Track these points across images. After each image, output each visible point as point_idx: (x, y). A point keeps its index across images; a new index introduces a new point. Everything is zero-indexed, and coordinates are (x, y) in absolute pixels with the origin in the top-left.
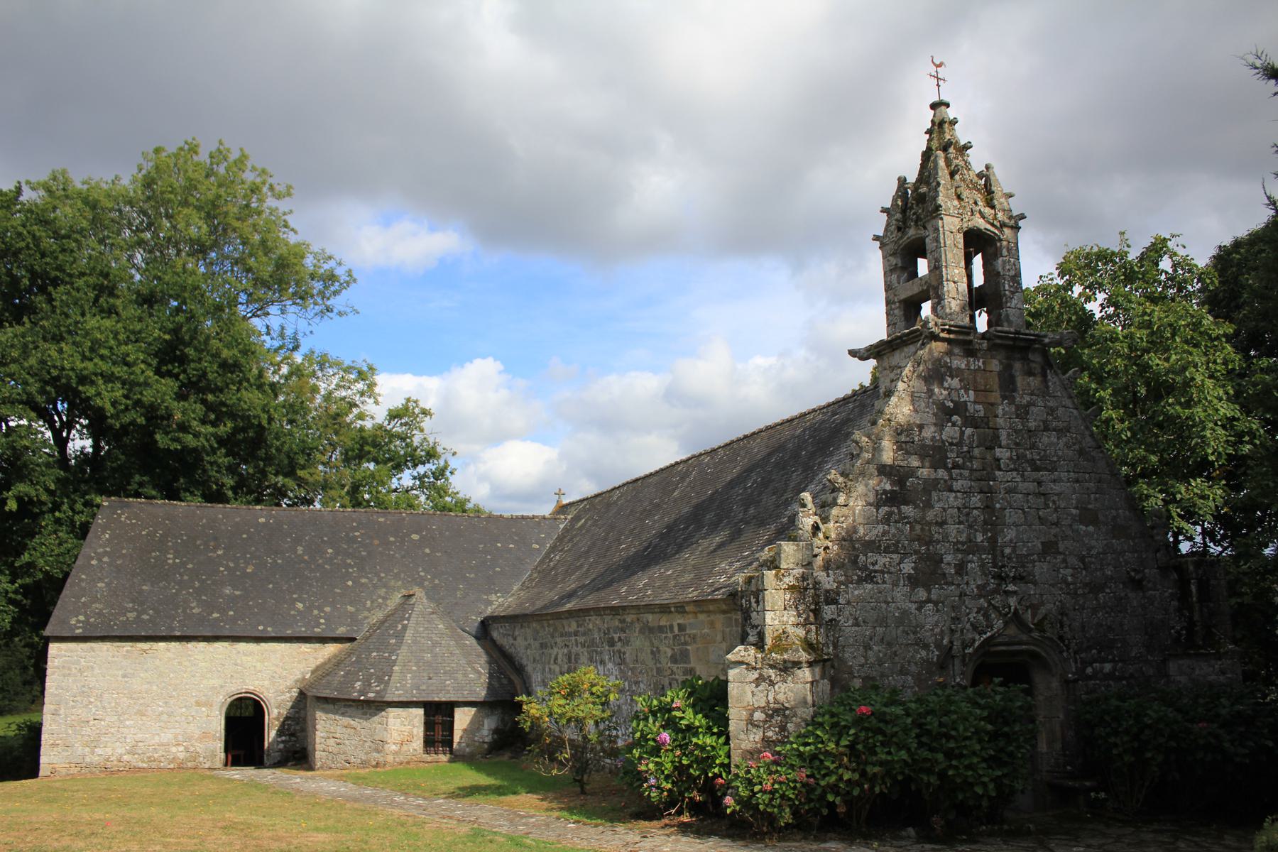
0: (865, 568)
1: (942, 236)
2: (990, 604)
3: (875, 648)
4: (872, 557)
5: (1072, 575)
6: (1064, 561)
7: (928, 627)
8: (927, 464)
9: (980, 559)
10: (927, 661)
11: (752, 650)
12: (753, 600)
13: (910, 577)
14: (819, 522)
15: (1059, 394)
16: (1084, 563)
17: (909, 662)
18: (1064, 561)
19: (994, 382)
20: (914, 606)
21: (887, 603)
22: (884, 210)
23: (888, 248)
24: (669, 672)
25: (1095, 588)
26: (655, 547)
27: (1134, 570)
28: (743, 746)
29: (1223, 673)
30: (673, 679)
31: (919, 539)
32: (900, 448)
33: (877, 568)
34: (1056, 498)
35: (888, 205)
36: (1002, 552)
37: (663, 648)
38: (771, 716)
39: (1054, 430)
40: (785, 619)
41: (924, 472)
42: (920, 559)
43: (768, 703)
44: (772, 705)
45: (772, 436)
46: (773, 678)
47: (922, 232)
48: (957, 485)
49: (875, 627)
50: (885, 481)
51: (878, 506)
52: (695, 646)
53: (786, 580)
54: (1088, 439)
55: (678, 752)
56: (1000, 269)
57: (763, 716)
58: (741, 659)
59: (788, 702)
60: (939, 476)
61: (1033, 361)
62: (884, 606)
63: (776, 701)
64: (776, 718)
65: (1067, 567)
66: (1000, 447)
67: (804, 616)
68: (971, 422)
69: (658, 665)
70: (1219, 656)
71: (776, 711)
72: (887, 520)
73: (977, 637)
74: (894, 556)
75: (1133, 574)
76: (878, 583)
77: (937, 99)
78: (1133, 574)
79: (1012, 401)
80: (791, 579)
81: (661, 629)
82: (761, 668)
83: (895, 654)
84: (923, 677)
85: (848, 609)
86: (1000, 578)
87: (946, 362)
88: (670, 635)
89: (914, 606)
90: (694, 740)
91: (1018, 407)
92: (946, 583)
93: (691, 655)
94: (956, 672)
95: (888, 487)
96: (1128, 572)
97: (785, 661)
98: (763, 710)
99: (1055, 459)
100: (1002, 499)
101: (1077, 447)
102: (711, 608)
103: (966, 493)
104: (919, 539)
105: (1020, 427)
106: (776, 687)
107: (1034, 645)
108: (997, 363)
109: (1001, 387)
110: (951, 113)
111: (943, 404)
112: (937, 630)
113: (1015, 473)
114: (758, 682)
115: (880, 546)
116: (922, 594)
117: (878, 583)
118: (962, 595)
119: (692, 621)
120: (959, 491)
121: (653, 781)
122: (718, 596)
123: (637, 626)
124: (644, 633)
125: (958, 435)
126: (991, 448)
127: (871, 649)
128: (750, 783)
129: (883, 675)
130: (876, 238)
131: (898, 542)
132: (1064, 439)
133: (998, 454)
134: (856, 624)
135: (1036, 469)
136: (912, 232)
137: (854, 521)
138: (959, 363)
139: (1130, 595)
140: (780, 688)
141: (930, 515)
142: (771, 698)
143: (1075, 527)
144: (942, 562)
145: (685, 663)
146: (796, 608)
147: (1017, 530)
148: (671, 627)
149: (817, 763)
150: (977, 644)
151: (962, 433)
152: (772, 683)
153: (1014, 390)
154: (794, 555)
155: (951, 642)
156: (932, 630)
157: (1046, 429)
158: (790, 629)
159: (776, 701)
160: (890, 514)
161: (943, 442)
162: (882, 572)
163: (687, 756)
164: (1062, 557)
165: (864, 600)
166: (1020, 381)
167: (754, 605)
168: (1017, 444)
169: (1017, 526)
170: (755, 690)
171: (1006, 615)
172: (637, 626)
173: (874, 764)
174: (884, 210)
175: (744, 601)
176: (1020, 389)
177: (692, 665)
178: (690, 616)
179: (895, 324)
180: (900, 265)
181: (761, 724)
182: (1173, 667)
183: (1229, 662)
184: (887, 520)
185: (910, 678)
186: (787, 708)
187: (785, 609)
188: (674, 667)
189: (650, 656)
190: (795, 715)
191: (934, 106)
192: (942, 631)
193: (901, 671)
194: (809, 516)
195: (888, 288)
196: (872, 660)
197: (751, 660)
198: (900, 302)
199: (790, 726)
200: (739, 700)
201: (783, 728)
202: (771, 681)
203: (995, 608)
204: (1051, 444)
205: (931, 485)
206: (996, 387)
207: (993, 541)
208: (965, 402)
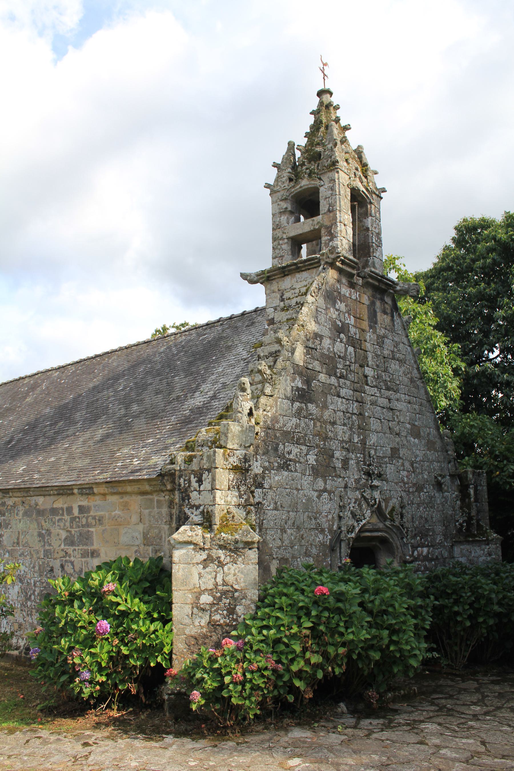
0: (282, 456)
1: (337, 186)
2: (363, 496)
3: (289, 531)
4: (289, 447)
5: (407, 477)
6: (403, 465)
7: (324, 514)
8: (324, 370)
9: (356, 456)
10: (323, 544)
11: (199, 530)
12: (193, 480)
13: (313, 467)
14: (253, 408)
15: (400, 332)
16: (413, 467)
17: (311, 545)
18: (403, 465)
19: (365, 314)
20: (316, 494)
21: (298, 490)
22: (275, 165)
23: (279, 195)
24: (62, 554)
25: (419, 488)
26: (20, 440)
27: (440, 475)
28: (187, 632)
29: (490, 555)
30: (66, 561)
31: (318, 434)
32: (308, 353)
33: (291, 457)
34: (398, 413)
35: (279, 162)
36: (369, 453)
37: (55, 530)
38: (220, 599)
39: (398, 360)
40: (229, 499)
41: (322, 377)
42: (319, 452)
43: (216, 585)
44: (220, 588)
45: (131, 354)
46: (222, 559)
47: (317, 183)
48: (343, 392)
49: (289, 512)
50: (298, 379)
51: (293, 401)
52: (100, 528)
53: (231, 460)
54: (415, 371)
55: (116, 641)
56: (370, 226)
57: (481, 600)
58: (190, 539)
59: (238, 583)
60: (332, 383)
61: (387, 303)
62: (295, 492)
63: (225, 583)
64: (224, 600)
65: (404, 470)
66: (368, 366)
67: (245, 497)
68: (352, 342)
69: (47, 547)
70: (488, 542)
71: (224, 593)
72: (298, 414)
73: (356, 524)
74: (303, 448)
75: (440, 478)
76: (292, 471)
77: (321, 87)
78: (440, 478)
79: (375, 332)
80: (235, 459)
81: (54, 511)
82: (210, 549)
83: (302, 537)
84: (320, 559)
85: (271, 493)
86: (369, 474)
87: (337, 287)
88: (66, 517)
89: (316, 494)
90: (134, 627)
91: (378, 336)
92: (336, 476)
93: (95, 538)
94: (342, 554)
95: (300, 385)
96: (436, 477)
97: (236, 542)
98: (210, 592)
99: (398, 382)
100: (369, 409)
101: (409, 376)
102: (129, 489)
103: (347, 399)
104: (318, 434)
105: (379, 353)
106: (226, 568)
107: (386, 532)
108: (367, 298)
109: (369, 318)
110: (335, 100)
111: (335, 322)
112: (330, 517)
113: (376, 389)
114: (205, 563)
115: (293, 437)
116: (320, 484)
117: (292, 471)
118: (346, 487)
119: (98, 502)
120: (343, 398)
121: (87, 675)
122: (144, 475)
123: (21, 509)
124: (30, 516)
125: (343, 350)
126: (362, 366)
127: (285, 532)
128: (218, 673)
129: (293, 557)
130: (268, 186)
131: (306, 435)
132: (403, 368)
133: (366, 372)
134: (276, 509)
135: (388, 389)
136: (305, 183)
137: (276, 411)
138: (345, 291)
139: (436, 495)
140: (229, 569)
141: (327, 414)
142: (219, 580)
143: (408, 438)
144: (334, 457)
145: (86, 545)
146: (238, 488)
147: (377, 436)
148: (69, 510)
149: (282, 647)
150: (357, 529)
151: (346, 349)
152: (221, 565)
153: (376, 323)
154: (239, 437)
155: (339, 528)
156: (327, 516)
157: (393, 358)
158: (234, 510)
159: (225, 583)
160: (300, 409)
161: (334, 353)
162: (295, 462)
163: (126, 645)
164: (401, 461)
165: (281, 486)
166: (380, 316)
167: (195, 484)
168: (377, 366)
169: (377, 432)
170: (202, 571)
171: (373, 506)
172: (21, 509)
173: (335, 645)
174: (275, 165)
175: (182, 480)
176: (379, 323)
177: (95, 547)
178: (97, 498)
179: (282, 257)
180: (289, 209)
181: (208, 607)
182: (457, 550)
183: (494, 546)
184: (298, 414)
185: (312, 559)
186: (236, 590)
187: (229, 489)
188: (70, 549)
189: (37, 539)
190: (245, 597)
191: (320, 94)
192: (333, 518)
193: (306, 553)
194: (247, 400)
195: (276, 227)
196: (286, 542)
197: (199, 540)
198: (288, 239)
199: (240, 609)
200: (185, 582)
201: (231, 611)
202: (219, 562)
203: (365, 499)
204: (396, 370)
205: (327, 390)
206: (366, 317)
207: (363, 442)
208: (348, 324)
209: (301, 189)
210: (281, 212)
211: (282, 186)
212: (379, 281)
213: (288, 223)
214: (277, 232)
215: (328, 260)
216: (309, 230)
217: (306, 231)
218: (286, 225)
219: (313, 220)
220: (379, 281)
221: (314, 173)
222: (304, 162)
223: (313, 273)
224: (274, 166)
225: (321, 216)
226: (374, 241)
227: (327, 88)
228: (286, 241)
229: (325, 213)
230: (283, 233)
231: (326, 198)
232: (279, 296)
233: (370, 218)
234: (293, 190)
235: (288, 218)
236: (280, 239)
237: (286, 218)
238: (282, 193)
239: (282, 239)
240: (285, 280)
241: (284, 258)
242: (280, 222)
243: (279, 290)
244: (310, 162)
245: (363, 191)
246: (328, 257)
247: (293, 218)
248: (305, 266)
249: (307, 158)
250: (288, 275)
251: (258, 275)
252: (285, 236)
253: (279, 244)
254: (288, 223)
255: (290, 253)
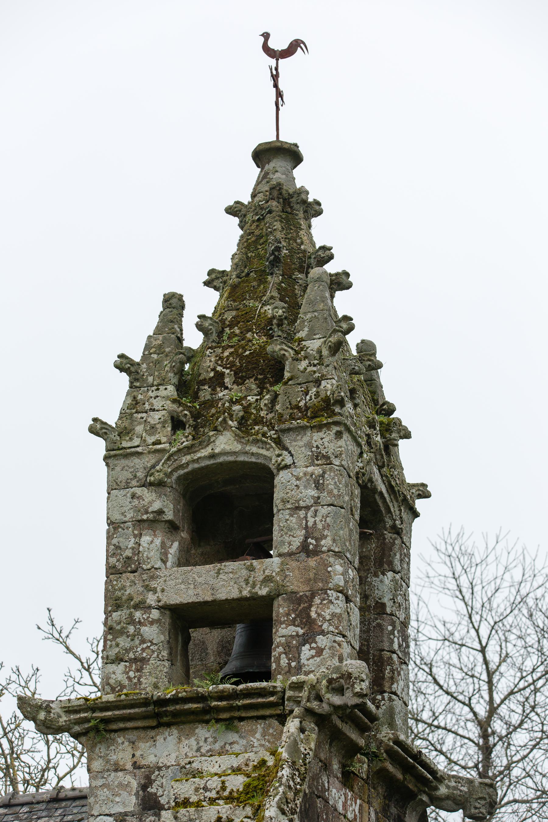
198: (164, 608)
209: (212, 462)
210: (141, 521)
211: (150, 440)
212: (407, 769)
213: (164, 562)
214: (127, 579)
215: (314, 705)
216: (235, 594)
217: (222, 595)
218: (159, 564)
219: (251, 569)
220: (407, 769)
221: (259, 421)
222: (221, 375)
223: (253, 732)
224: (120, 367)
225: (276, 560)
226: (396, 647)
227: (286, 137)
228: (155, 614)
229: (290, 554)
230: (148, 588)
231: (298, 508)
232: (134, 784)
233: (390, 574)
234: (185, 459)
235: (163, 544)
236: (136, 607)
237: (158, 542)
238: (149, 460)
239: (141, 606)
240: (160, 739)
241: (147, 669)
242: (136, 551)
243: (136, 766)
244: (239, 380)
245: (381, 493)
246: (319, 698)
247: (176, 545)
248: (231, 708)
249: (231, 366)
250: (168, 725)
251: (69, 710)
252: (151, 599)
253: (131, 621)
254: (164, 562)
255: (165, 653)
